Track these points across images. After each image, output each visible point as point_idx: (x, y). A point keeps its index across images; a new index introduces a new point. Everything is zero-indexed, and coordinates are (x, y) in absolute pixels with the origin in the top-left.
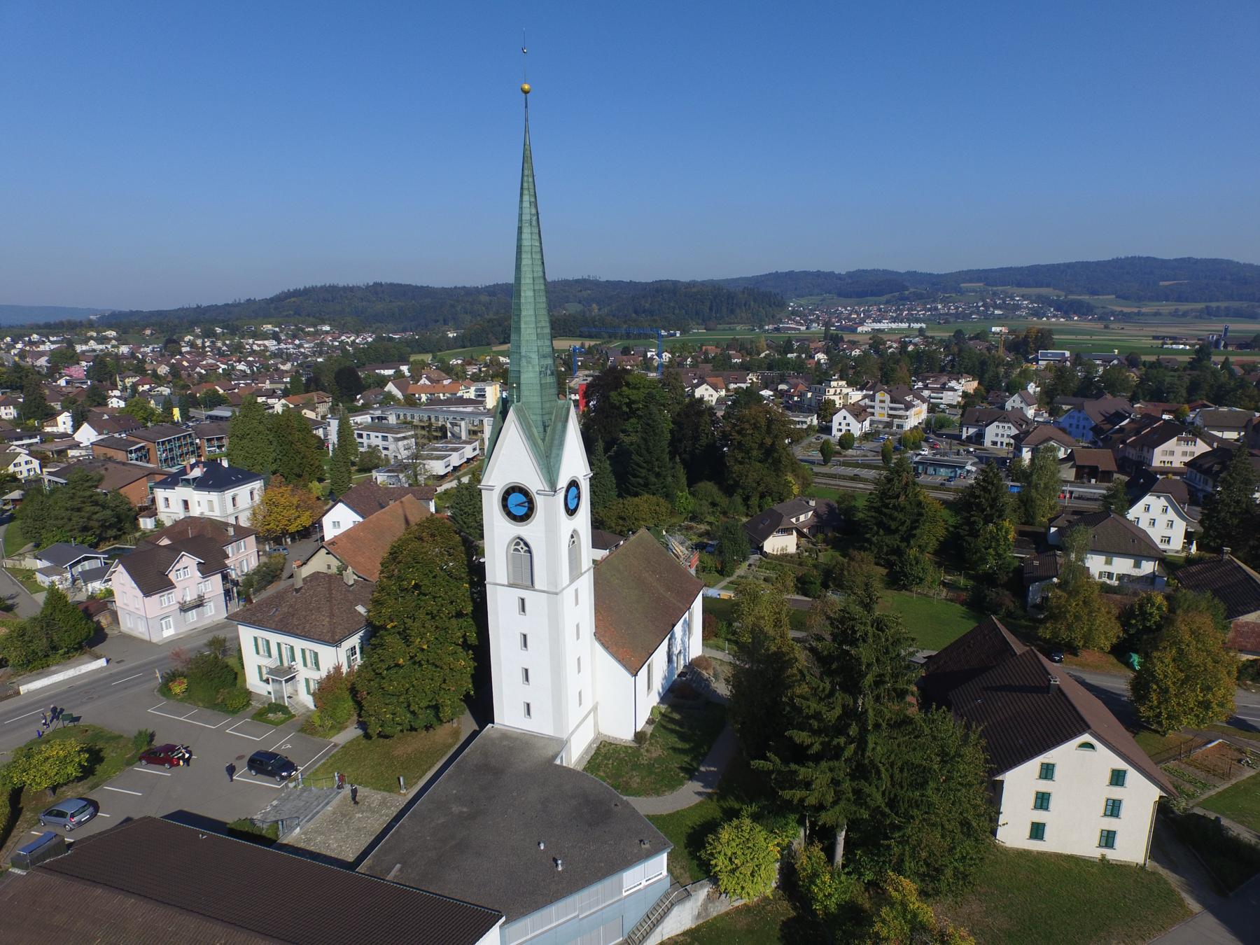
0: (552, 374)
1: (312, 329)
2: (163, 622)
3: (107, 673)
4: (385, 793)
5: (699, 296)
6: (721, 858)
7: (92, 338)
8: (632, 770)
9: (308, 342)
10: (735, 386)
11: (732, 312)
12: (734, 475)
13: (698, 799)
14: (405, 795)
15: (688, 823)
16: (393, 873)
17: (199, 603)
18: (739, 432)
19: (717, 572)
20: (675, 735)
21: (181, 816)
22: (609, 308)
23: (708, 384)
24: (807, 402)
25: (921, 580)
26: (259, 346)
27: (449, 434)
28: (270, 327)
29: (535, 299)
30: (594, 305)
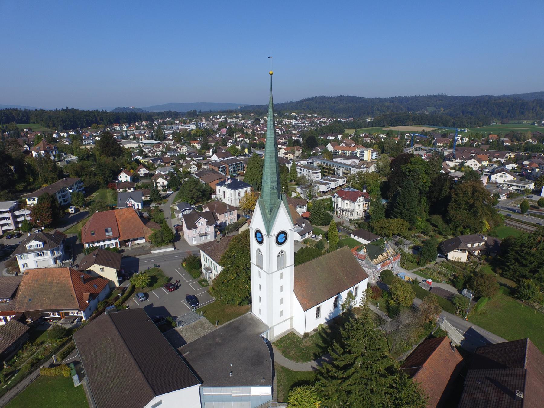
0: (276, 189)
1: (310, 116)
2: (193, 239)
3: (173, 253)
4: (211, 324)
5: (502, 105)
6: (292, 398)
7: (234, 117)
8: (294, 348)
9: (307, 121)
10: (497, 159)
11: (522, 113)
12: (450, 215)
13: (311, 370)
14: (216, 327)
15: (298, 378)
16: (186, 354)
17: (205, 235)
18: (456, 195)
19: (417, 263)
20: (321, 339)
21: (537, 224)
22: (449, 110)
23: (475, 159)
24: (534, 174)
25: (529, 298)
26: (288, 122)
27: (335, 173)
28: (294, 114)
29: (270, 159)
30: (442, 108)
